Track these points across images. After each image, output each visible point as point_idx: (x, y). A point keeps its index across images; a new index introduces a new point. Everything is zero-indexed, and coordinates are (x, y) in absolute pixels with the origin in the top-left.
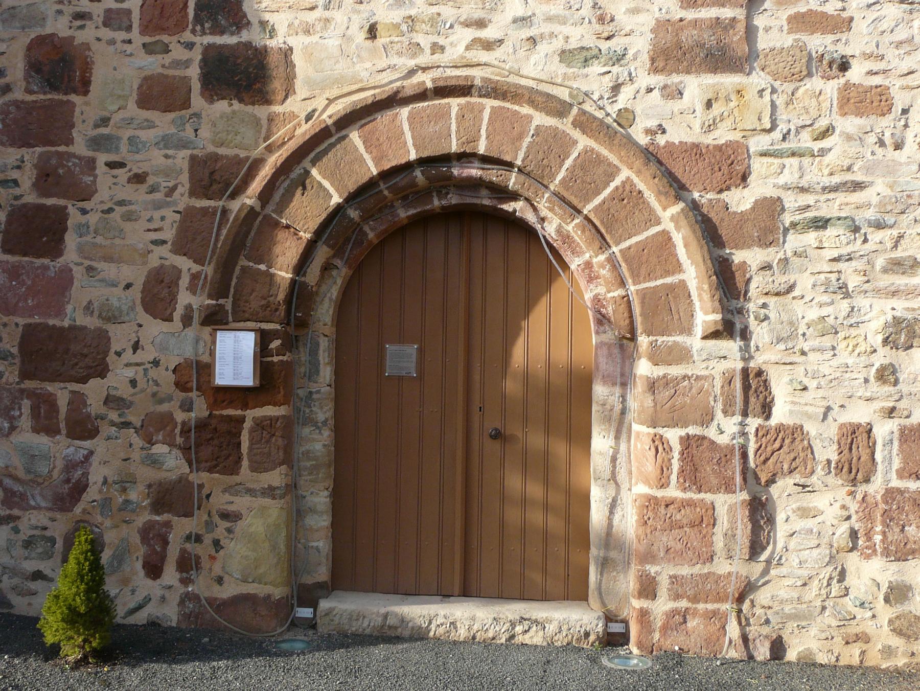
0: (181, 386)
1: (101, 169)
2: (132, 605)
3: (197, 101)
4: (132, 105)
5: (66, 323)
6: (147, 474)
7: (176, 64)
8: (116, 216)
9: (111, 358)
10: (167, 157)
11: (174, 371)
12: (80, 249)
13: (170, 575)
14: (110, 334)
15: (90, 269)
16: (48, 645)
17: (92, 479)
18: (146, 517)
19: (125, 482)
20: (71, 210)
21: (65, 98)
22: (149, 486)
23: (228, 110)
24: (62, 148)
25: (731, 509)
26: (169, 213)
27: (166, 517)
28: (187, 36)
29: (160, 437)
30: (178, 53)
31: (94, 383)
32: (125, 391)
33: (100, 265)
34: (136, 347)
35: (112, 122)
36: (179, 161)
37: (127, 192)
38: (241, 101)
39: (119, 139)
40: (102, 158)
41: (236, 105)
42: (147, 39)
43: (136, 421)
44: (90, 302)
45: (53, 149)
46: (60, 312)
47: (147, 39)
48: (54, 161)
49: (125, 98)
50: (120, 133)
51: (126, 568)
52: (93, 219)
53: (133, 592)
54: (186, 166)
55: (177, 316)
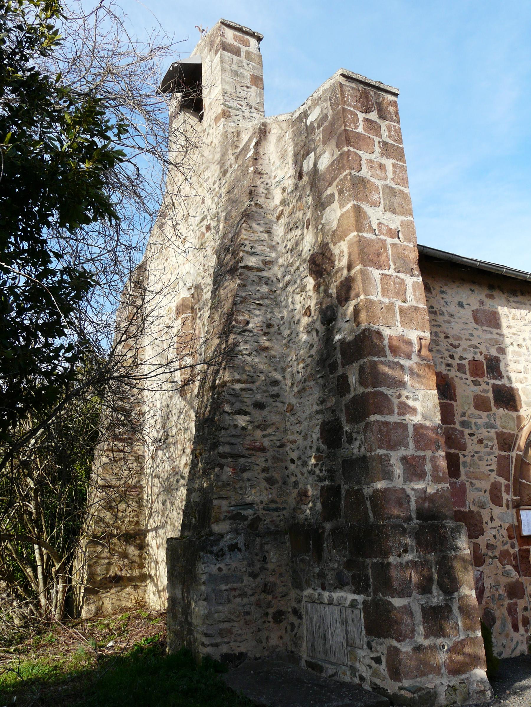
0: (510, 537)
1: (467, 436)
2: (513, 647)
3: (494, 408)
4: (472, 408)
5: (467, 510)
6: (504, 580)
7: (485, 391)
8: (476, 458)
9: (484, 525)
10: (488, 432)
11: (507, 530)
12: (466, 475)
13: (521, 629)
14: (482, 514)
15: (471, 483)
16: (526, 653)
17: (485, 586)
18: (507, 602)
19: (497, 585)
20: (460, 455)
21: (450, 402)
22: (505, 586)
23: (504, 413)
24: (452, 426)
25: (414, 285)
26: (492, 457)
27: (515, 600)
28: (486, 379)
29: (506, 562)
30: (484, 386)
31: (481, 537)
32: (493, 541)
33: (474, 481)
34: (492, 519)
35: (467, 415)
36: (492, 434)
37: (477, 447)
38: (507, 409)
39: (471, 422)
40: (466, 431)
41: (506, 411)
42: (473, 379)
43: (497, 554)
44: (474, 499)
45: (449, 426)
46: (464, 505)
47: (473, 379)
48: (450, 432)
49: (469, 404)
50: (471, 420)
51: (507, 629)
52: (468, 459)
53: (512, 640)
54: (494, 436)
55: (504, 504)
